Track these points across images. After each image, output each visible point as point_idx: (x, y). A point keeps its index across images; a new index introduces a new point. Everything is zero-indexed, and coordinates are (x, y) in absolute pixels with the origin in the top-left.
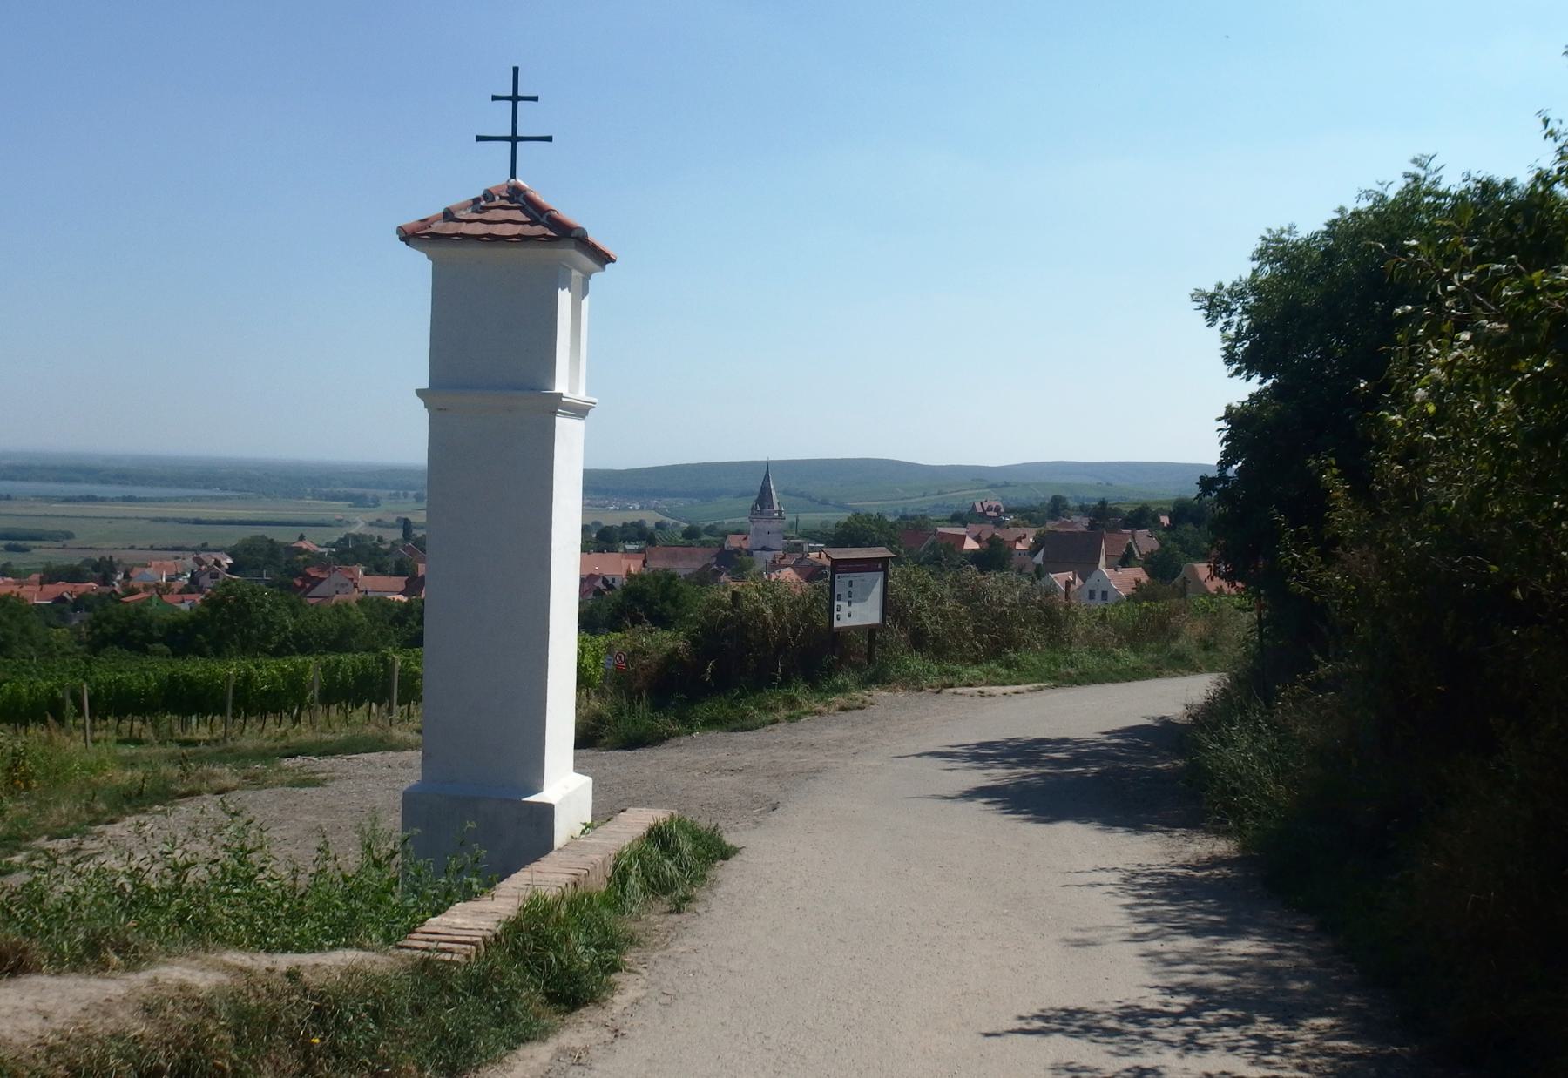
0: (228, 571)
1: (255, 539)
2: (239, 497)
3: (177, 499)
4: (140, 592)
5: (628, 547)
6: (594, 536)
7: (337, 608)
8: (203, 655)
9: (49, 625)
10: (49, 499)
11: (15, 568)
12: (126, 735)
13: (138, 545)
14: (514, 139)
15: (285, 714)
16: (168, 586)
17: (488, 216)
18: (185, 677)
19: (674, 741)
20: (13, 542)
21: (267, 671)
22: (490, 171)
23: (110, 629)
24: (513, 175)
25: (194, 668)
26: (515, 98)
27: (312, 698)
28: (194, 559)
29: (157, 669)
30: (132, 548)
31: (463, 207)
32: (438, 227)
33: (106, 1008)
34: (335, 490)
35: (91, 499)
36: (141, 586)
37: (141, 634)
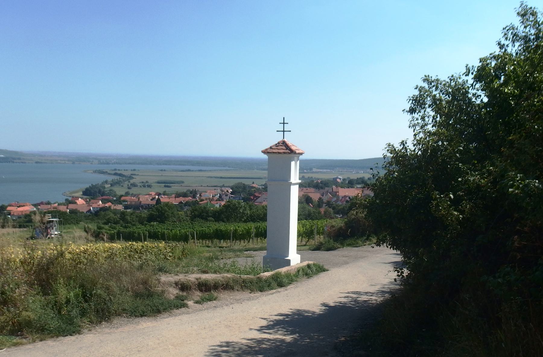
0: (231, 194)
1: (239, 183)
2: (234, 170)
3: (215, 170)
4: (204, 201)
5: (358, 186)
6: (347, 182)
7: (263, 207)
8: (223, 221)
9: (178, 211)
10: (176, 171)
11: (167, 193)
12: (205, 245)
13: (203, 185)
14: (284, 131)
15: (246, 240)
16: (213, 199)
17: (278, 148)
18: (220, 229)
19: (339, 249)
20: (166, 184)
21: (241, 227)
22: (279, 138)
23: (197, 213)
24: (284, 138)
25: (222, 226)
26: (284, 123)
27: (253, 236)
28: (220, 190)
29: (213, 226)
30: (202, 186)
31: (273, 146)
32: (268, 151)
33: (218, 277)
34: (264, 167)
35: (189, 170)
36: (205, 198)
37: (206, 214)
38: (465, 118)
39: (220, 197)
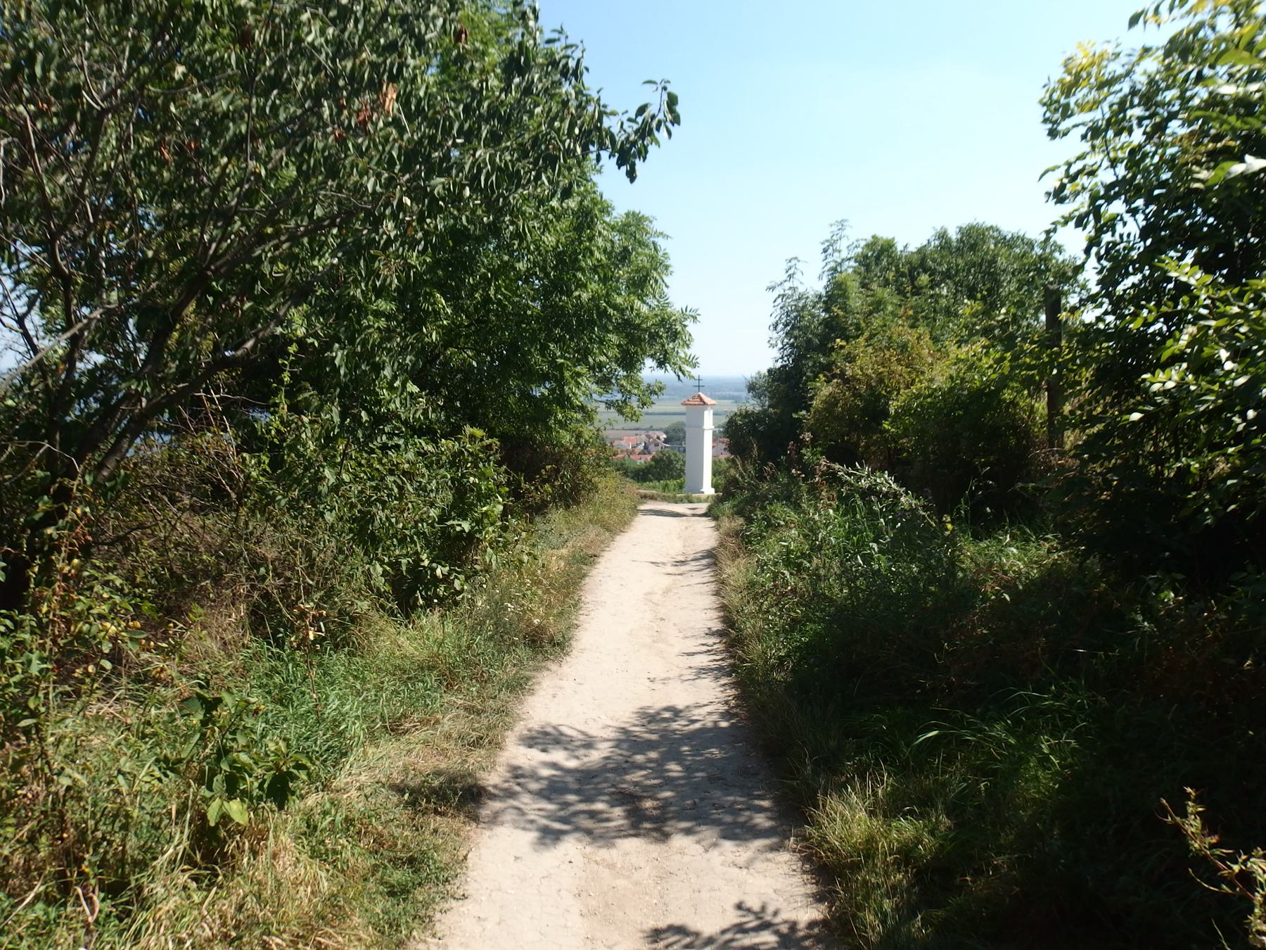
38: (1055, 372)
39: (646, 447)
